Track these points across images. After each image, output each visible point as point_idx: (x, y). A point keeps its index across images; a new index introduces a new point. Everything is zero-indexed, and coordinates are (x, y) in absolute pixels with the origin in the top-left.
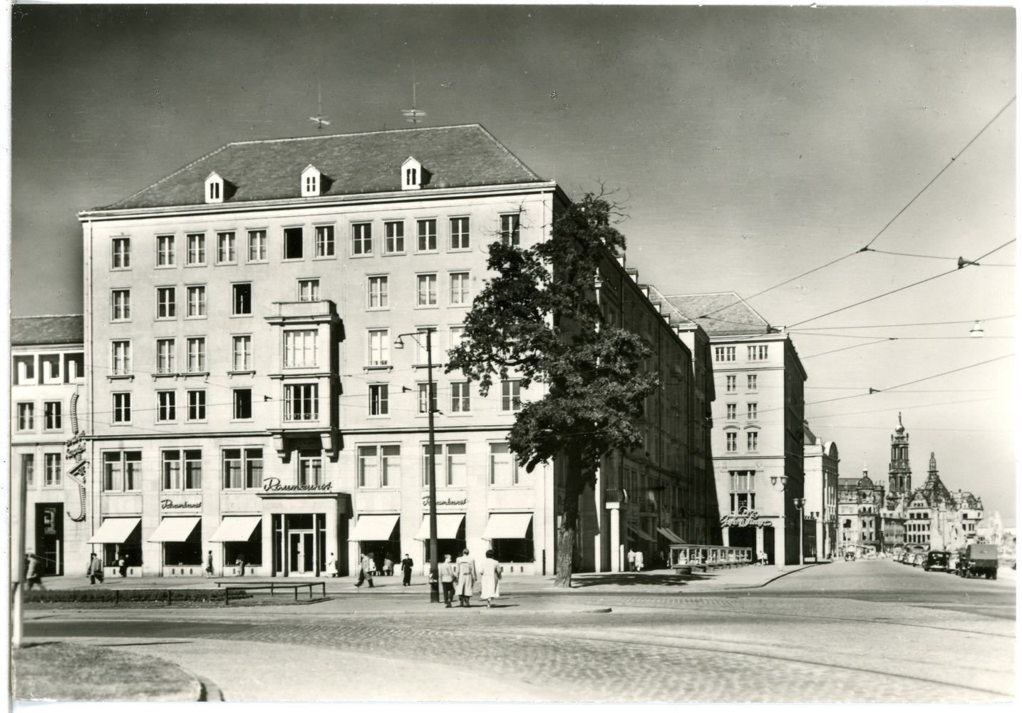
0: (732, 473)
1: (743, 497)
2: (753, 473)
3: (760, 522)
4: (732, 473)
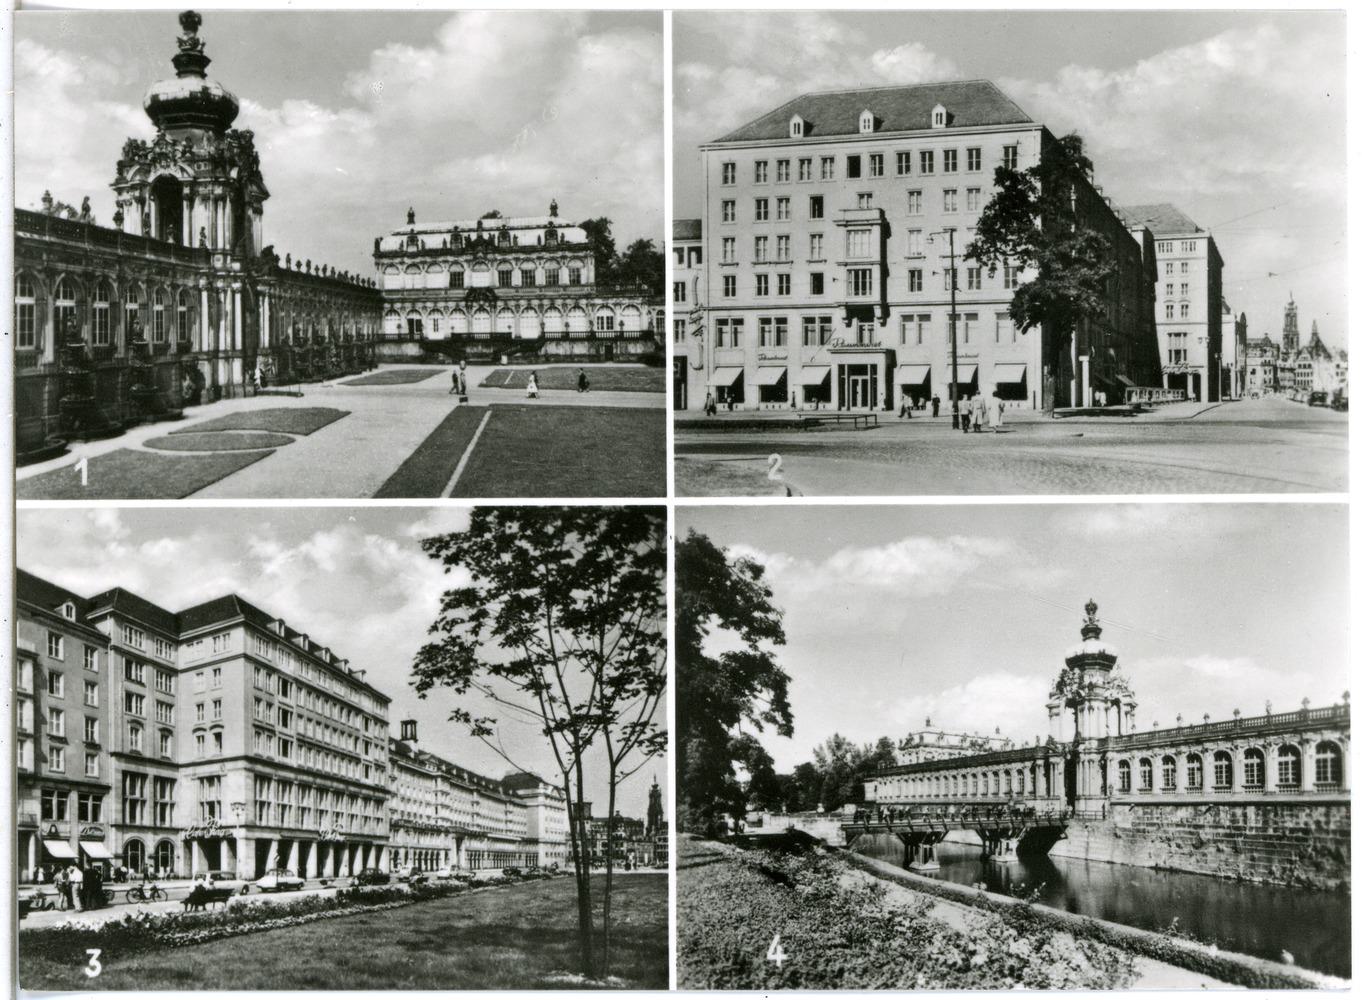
0: (201, 779)
1: (211, 806)
2: (219, 777)
3: (221, 833)
4: (201, 779)
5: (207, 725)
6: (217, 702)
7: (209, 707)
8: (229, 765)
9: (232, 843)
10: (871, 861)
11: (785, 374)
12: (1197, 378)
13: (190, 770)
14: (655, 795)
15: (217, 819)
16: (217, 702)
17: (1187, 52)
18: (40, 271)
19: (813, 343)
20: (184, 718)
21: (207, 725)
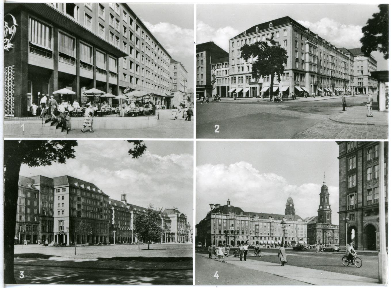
0: (358, 79)
1: (360, 83)
2: (362, 78)
3: (363, 87)
4: (358, 79)
5: (360, 70)
6: (63, 211)
7: (360, 67)
8: (364, 77)
9: (365, 89)
10: (53, 36)
11: (289, 88)
12: (66, 236)
13: (356, 77)
14: (324, 194)
15: (362, 85)
16: (63, 211)
17: (189, 155)
18: (268, 58)
19: (60, 4)
20: (355, 69)
21: (360, 70)
